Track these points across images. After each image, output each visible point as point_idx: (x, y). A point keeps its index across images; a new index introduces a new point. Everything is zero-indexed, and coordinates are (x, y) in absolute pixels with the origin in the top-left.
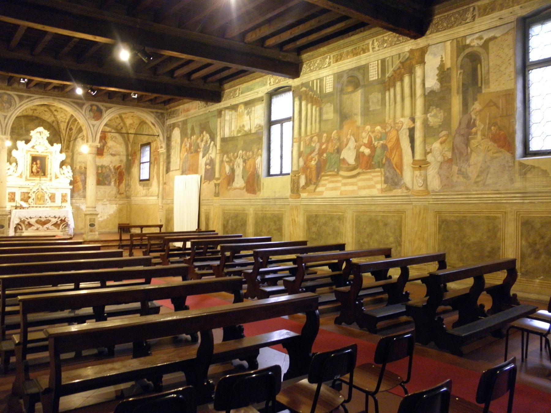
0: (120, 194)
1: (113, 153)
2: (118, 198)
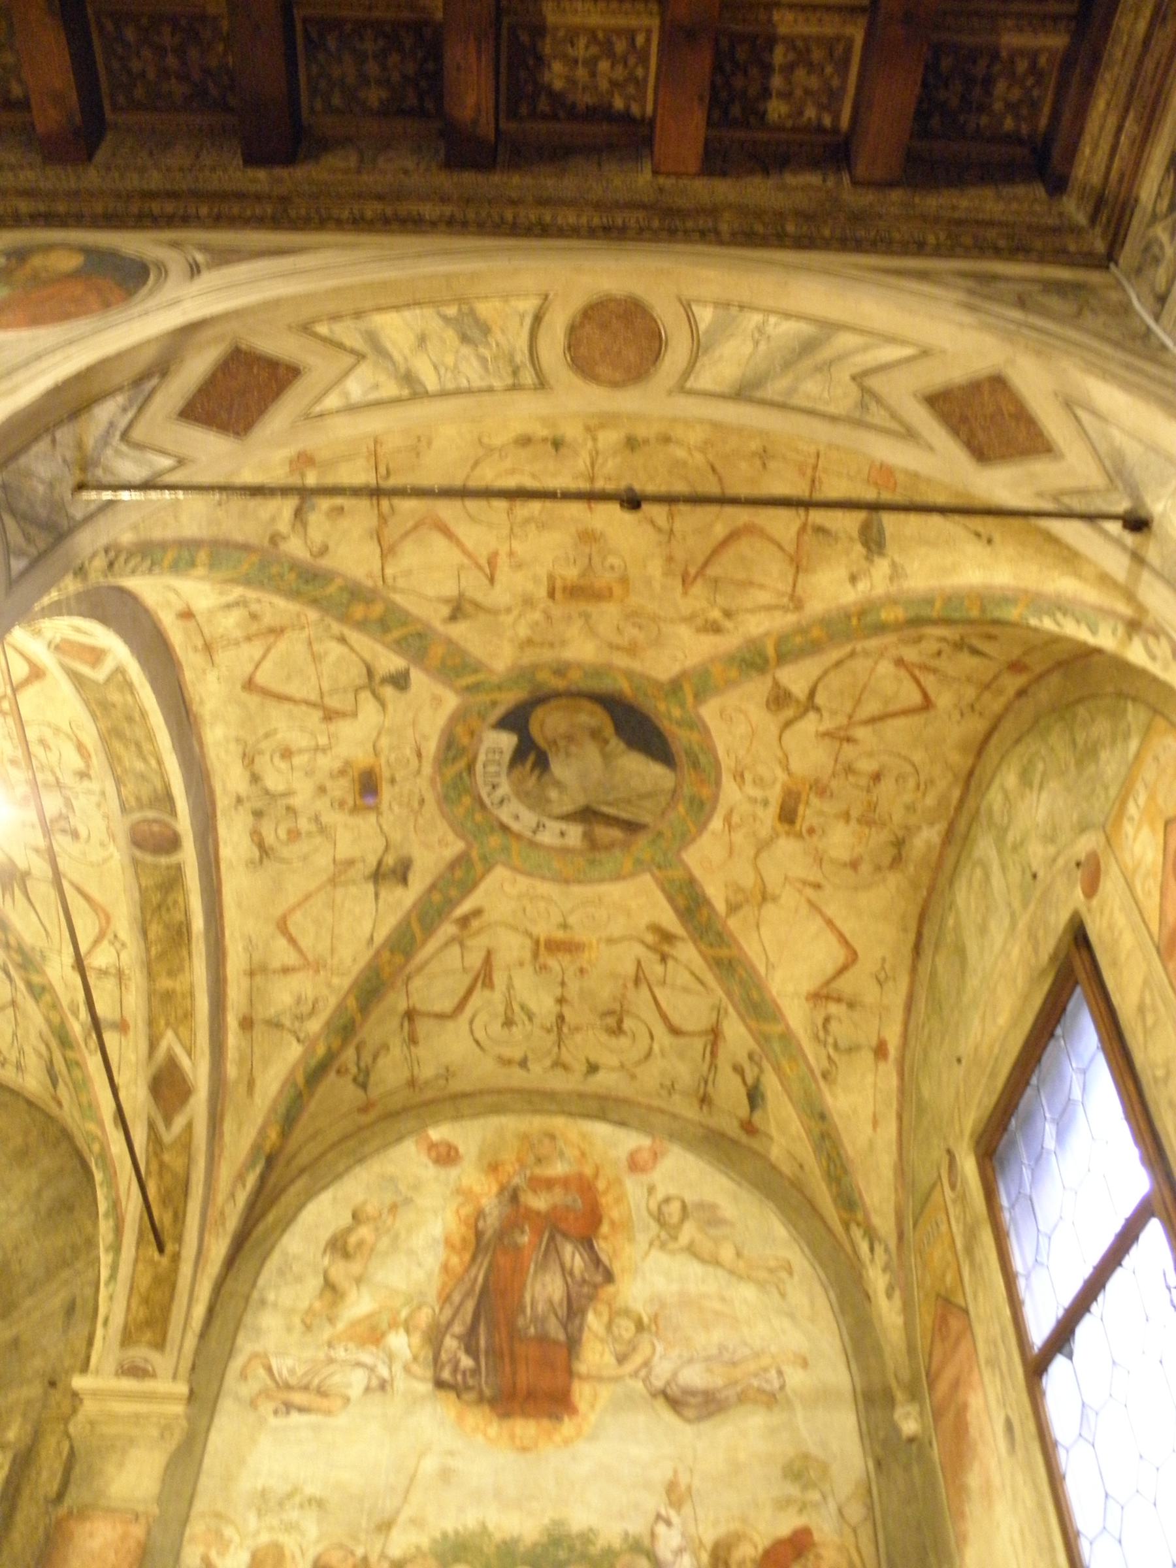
1: (694, 1377)
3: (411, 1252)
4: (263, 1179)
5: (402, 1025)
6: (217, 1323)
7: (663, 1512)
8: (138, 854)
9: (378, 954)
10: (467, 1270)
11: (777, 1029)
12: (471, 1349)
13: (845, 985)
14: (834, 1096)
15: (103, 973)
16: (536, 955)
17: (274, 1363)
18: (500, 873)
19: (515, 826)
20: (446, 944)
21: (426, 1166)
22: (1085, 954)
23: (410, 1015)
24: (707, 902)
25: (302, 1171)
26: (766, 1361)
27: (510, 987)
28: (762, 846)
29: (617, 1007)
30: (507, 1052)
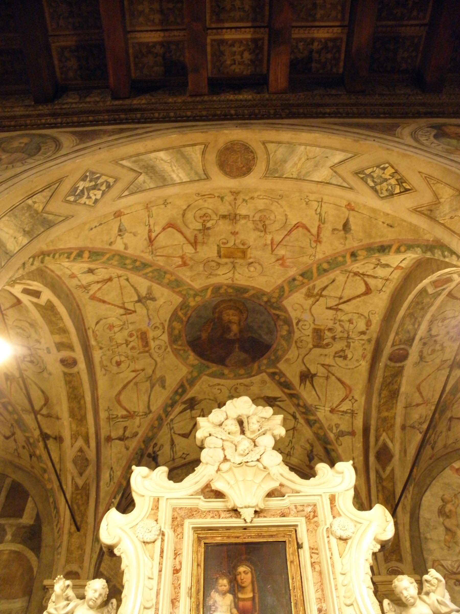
17: (444, 563)
23: (451, 419)
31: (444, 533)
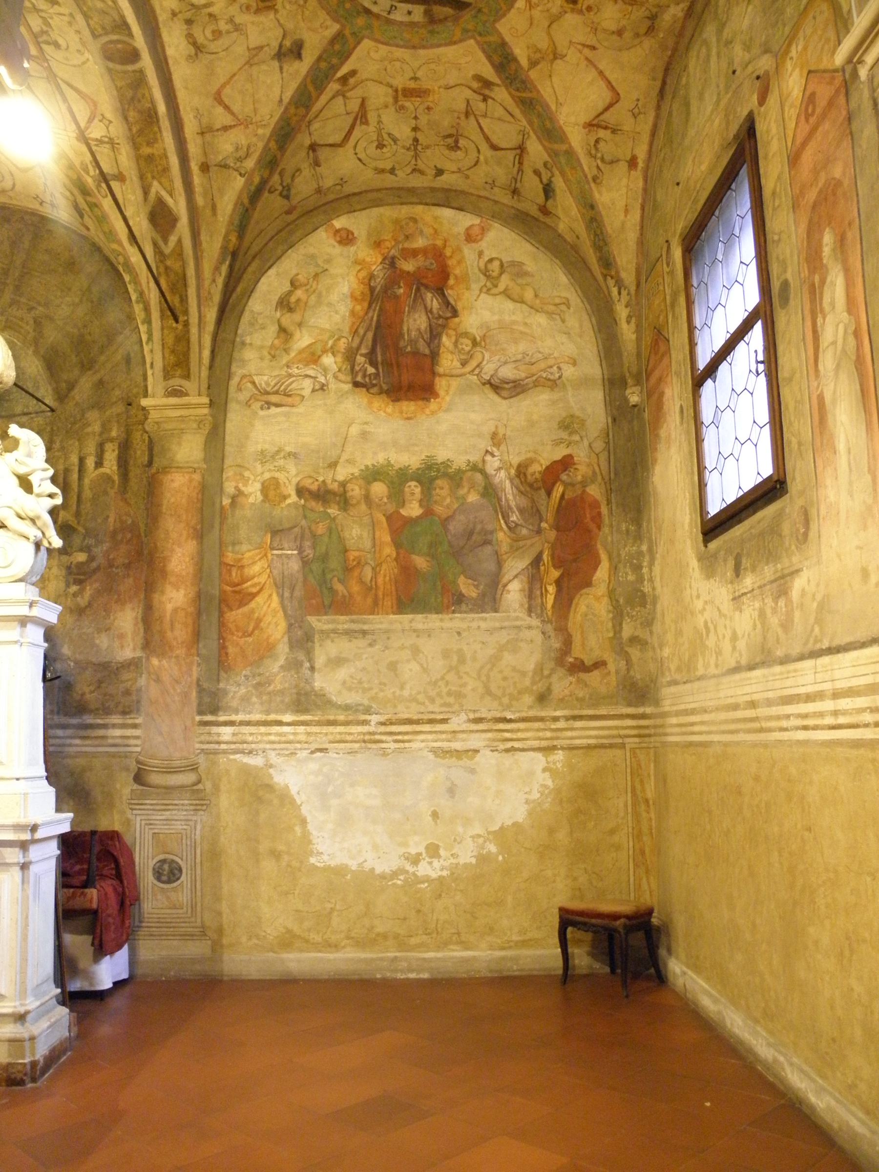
0: (579, 667)
1: (507, 372)
2: (562, 702)
3: (330, 304)
4: (231, 267)
5: (308, 153)
6: (218, 360)
7: (489, 449)
8: (111, 65)
9: (286, 109)
10: (366, 313)
11: (564, 147)
12: (373, 363)
13: (610, 117)
14: (600, 193)
15: (100, 142)
16: (396, 99)
17: (256, 379)
18: (366, 43)
19: (375, 9)
20: (334, 97)
21: (334, 246)
22: (752, 142)
23: (313, 147)
24: (515, 60)
25: (254, 257)
26: (551, 362)
27: (379, 122)
28: (554, 20)
29: (454, 131)
30: (381, 165)
31: (275, 335)
